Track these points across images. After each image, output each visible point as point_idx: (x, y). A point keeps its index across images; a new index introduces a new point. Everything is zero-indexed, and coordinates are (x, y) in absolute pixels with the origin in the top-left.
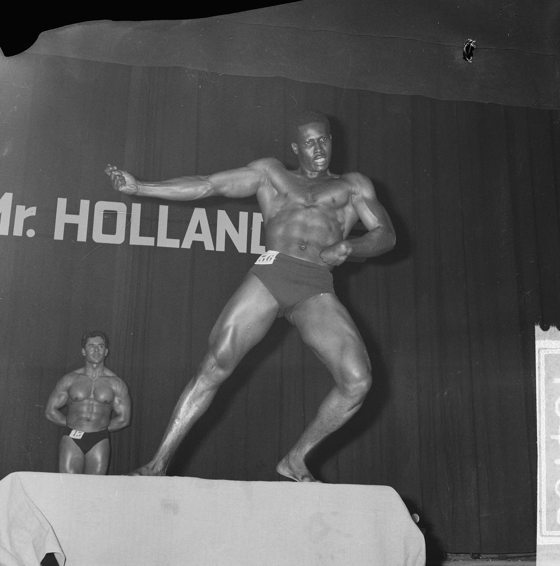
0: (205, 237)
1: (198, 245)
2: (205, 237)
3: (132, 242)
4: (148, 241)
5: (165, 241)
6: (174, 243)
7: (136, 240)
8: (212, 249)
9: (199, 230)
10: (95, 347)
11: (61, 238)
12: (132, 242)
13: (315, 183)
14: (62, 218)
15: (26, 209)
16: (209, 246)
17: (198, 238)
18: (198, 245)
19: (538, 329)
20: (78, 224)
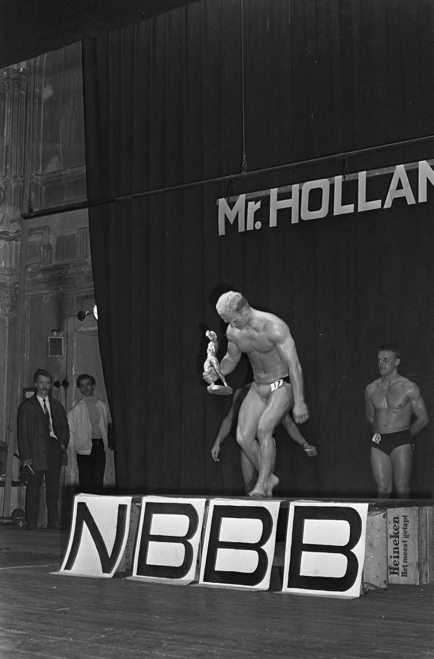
0: (406, 192)
1: (400, 202)
2: (406, 192)
3: (336, 213)
4: (349, 208)
5: (364, 206)
6: (376, 204)
7: (340, 209)
8: (414, 202)
9: (400, 187)
10: (387, 357)
11: (224, 233)
12: (336, 213)
13: (115, 199)
14: (275, 205)
15: (255, 203)
16: (411, 201)
17: (400, 194)
18: (400, 202)
19: (189, 541)
20: (278, 210)
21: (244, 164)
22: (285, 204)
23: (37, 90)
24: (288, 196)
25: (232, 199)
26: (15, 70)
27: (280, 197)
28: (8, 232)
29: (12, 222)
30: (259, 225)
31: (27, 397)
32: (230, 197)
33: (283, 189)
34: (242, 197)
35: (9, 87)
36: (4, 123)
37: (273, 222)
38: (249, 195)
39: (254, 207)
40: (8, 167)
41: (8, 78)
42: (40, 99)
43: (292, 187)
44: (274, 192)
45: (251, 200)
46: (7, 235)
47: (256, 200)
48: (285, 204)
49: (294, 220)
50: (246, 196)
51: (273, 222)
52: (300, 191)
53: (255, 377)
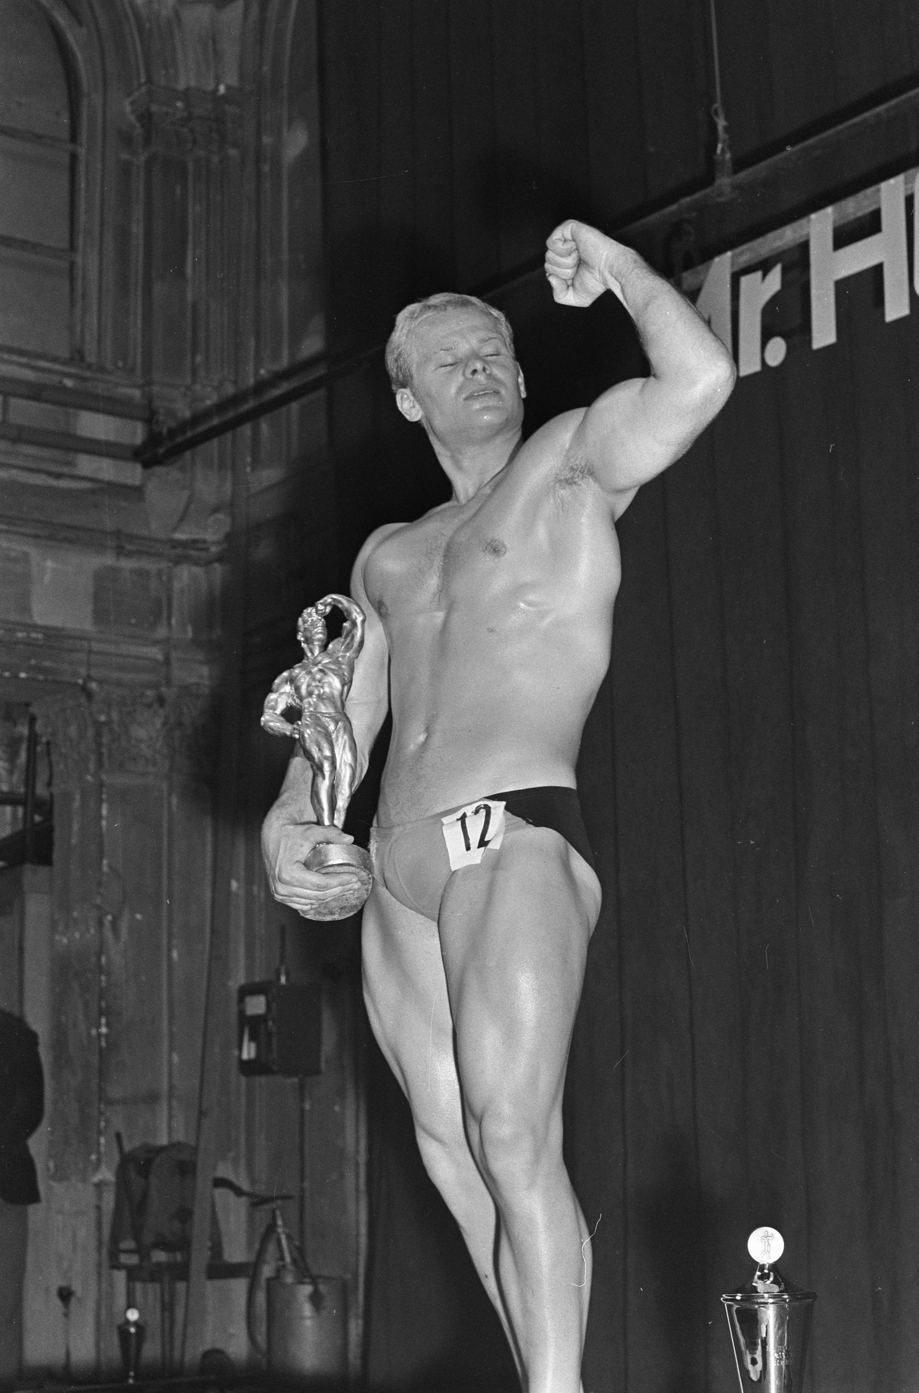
14: (831, 267)
21: (723, 150)
22: (857, 258)
23: (267, 140)
24: (870, 225)
25: (688, 278)
26: (205, 92)
27: (845, 236)
28: (205, 542)
29: (215, 510)
30: (777, 351)
31: (262, 999)
32: (684, 275)
33: (854, 207)
34: (722, 266)
35: (195, 141)
36: (184, 242)
37: (824, 332)
38: (741, 254)
39: (763, 288)
40: (199, 358)
41: (189, 118)
42: (276, 161)
43: (878, 191)
44: (820, 226)
45: (748, 270)
46: (202, 549)
47: (764, 266)
48: (857, 258)
49: (896, 308)
50: (733, 257)
51: (824, 332)
52: (909, 201)
53: (282, 719)
